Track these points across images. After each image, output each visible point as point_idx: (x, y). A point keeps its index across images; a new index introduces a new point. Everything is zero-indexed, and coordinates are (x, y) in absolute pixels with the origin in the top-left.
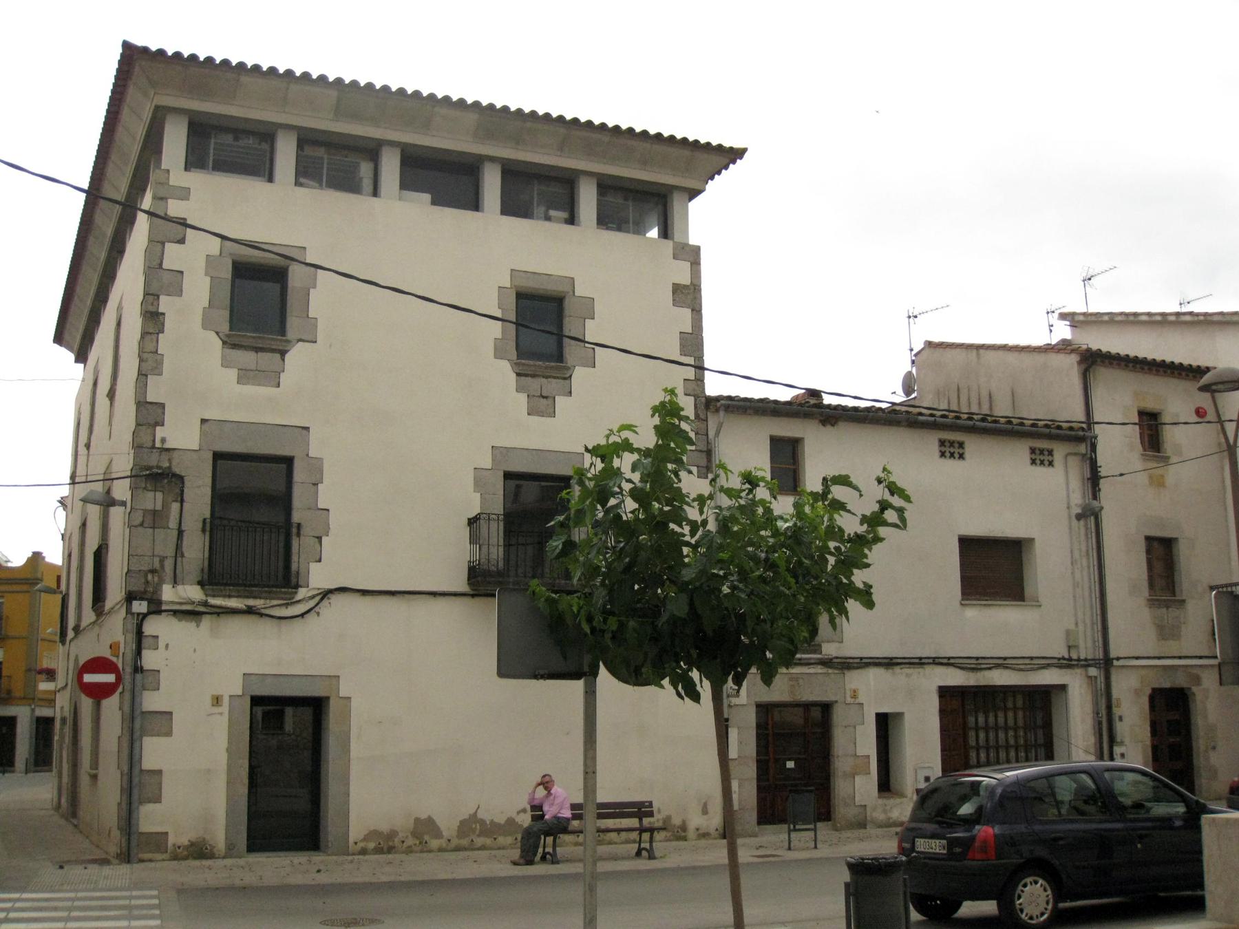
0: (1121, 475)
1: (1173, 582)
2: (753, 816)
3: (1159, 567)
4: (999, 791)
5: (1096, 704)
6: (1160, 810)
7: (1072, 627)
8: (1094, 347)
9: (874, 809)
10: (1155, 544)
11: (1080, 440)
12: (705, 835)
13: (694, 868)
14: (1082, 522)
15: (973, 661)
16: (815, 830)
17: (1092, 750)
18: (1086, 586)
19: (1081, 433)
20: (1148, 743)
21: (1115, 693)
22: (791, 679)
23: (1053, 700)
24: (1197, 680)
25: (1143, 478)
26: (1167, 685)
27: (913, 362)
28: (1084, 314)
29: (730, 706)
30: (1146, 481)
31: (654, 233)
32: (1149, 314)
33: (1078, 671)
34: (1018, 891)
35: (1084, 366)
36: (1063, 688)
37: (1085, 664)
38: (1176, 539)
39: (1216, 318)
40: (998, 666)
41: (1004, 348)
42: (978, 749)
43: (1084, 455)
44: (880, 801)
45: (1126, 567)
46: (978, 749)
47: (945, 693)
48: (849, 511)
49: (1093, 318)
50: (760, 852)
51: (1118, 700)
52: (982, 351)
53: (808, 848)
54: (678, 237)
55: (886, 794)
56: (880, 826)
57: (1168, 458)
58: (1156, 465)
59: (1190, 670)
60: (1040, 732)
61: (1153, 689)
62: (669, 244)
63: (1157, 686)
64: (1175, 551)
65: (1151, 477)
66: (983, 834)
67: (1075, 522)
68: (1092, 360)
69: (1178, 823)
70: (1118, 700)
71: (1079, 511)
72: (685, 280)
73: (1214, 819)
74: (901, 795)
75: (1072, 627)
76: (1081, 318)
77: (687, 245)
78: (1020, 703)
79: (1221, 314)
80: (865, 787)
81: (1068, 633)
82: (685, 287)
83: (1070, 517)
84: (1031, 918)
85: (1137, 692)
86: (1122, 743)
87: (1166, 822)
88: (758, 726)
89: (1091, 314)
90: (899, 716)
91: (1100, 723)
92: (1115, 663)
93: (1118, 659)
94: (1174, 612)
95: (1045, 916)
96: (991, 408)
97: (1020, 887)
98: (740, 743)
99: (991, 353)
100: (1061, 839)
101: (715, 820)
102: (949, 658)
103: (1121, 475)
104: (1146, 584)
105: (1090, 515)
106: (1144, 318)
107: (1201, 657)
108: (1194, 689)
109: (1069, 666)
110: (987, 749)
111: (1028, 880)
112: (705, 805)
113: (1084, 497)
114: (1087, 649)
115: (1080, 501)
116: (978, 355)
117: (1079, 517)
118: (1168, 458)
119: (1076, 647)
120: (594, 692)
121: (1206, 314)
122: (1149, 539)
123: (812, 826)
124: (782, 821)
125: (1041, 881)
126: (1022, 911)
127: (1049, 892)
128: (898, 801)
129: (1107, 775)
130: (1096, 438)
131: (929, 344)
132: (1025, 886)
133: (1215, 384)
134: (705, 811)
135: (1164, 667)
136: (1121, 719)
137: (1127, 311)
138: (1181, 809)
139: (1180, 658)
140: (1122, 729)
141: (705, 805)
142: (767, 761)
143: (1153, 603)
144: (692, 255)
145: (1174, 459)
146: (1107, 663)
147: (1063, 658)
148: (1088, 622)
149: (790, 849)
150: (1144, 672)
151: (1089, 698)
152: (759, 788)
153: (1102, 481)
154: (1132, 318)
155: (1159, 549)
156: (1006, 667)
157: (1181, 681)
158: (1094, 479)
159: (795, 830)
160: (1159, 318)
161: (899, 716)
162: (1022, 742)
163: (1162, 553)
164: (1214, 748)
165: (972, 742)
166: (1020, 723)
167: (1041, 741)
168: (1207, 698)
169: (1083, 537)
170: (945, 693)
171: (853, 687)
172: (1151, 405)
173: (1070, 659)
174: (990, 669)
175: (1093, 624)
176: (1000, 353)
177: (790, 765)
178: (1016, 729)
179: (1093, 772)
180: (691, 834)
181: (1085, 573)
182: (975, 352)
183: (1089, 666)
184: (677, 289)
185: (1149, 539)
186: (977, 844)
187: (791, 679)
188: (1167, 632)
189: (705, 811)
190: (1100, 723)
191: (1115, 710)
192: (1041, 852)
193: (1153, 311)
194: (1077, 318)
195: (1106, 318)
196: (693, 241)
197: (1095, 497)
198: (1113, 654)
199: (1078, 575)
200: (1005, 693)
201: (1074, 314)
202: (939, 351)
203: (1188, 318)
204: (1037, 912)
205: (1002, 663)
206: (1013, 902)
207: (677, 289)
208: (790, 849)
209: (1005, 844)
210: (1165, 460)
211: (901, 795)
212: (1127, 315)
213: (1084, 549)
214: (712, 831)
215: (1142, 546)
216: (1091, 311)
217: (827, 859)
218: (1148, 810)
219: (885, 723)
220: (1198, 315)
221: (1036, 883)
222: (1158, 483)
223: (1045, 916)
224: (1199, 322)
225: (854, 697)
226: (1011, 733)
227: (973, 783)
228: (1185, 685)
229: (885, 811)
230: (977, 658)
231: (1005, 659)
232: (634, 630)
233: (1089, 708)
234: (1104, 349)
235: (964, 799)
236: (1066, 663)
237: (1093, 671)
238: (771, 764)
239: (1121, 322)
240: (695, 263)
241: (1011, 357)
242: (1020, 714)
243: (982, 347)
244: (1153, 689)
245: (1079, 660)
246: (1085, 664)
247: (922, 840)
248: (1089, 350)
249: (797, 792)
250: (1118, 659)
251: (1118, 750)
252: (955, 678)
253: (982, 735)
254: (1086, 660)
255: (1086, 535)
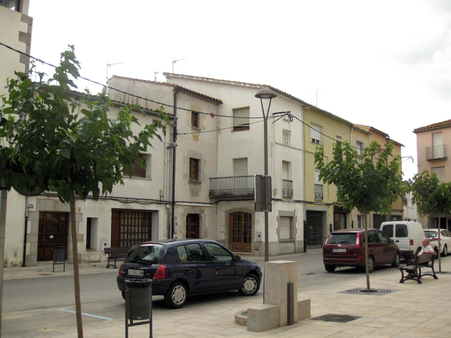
0: (185, 134)
1: (197, 176)
2: (35, 257)
3: (193, 169)
4: (166, 251)
5: (168, 218)
6: (220, 259)
7: (162, 189)
8: (180, 85)
9: (84, 255)
10: (192, 161)
11: (171, 119)
12: (15, 265)
13: (15, 280)
14: (169, 150)
15: (126, 199)
16: (64, 264)
17: (166, 235)
18: (168, 174)
19: (172, 117)
20: (185, 233)
21: (175, 215)
22: (54, 202)
23: (153, 215)
24: (203, 212)
25: (191, 136)
26: (193, 213)
27: (107, 82)
28: (173, 74)
29: (28, 212)
30: (192, 137)
31: (13, 9)
32: (197, 77)
33: (163, 206)
34: (173, 291)
35: (175, 92)
36: (157, 211)
37: (166, 203)
38: (200, 160)
39: (221, 82)
40: (134, 202)
41: (145, 81)
42: (124, 233)
43: (172, 125)
44: (87, 253)
45: (183, 168)
46: (124, 233)
47: (115, 211)
48: (138, 123)
49: (176, 76)
50: (41, 273)
51: (176, 217)
52: (136, 81)
53: (60, 271)
54: (24, 12)
55: (88, 250)
56: (86, 262)
57: (200, 130)
58: (195, 132)
59: (201, 208)
60: (147, 228)
61: (188, 214)
62: (19, 15)
63: (189, 213)
64: (199, 164)
65: (194, 137)
66: (159, 268)
67: (166, 149)
68: (178, 90)
69: (228, 264)
70: (176, 217)
71: (169, 146)
72: (25, 31)
73: (271, 263)
74: (95, 250)
75: (162, 189)
76: (172, 75)
77: (28, 16)
78: (140, 216)
79: (223, 80)
80: (81, 246)
81: (160, 191)
82: (24, 34)
83: (165, 148)
84: (177, 302)
85: (183, 215)
86: (176, 233)
87: (222, 264)
88: (40, 220)
89: (175, 74)
90: (96, 219)
91: (169, 225)
92: (176, 203)
93: (177, 202)
94: (197, 186)
95: (183, 301)
96: (137, 103)
97: (174, 290)
98: (32, 227)
99: (140, 83)
100: (190, 270)
101: (20, 259)
102: (117, 198)
103: (185, 134)
104: (188, 175)
105: (172, 148)
106: (195, 78)
107: (205, 203)
108: (202, 215)
109: (160, 204)
110: (127, 233)
111: (177, 287)
112: (16, 253)
113: (170, 141)
114: (167, 197)
115: (169, 142)
116: (134, 83)
117: (168, 148)
118: (200, 130)
119: (163, 196)
120: (6, 198)
121: (218, 80)
122: (191, 159)
123: (63, 262)
124: (51, 259)
125: (181, 287)
126: (174, 299)
127: (184, 292)
128: (94, 252)
129: (205, 244)
130: (177, 119)
131: (115, 76)
132: (176, 289)
133: (264, 94)
134: (15, 255)
135: (193, 206)
136: (176, 224)
137: (189, 75)
138: (230, 258)
139: (198, 203)
140: (177, 228)
141: (16, 253)
142: (42, 235)
143: (191, 182)
144: (29, 21)
145: (202, 131)
146: (173, 203)
147: (158, 200)
148: (168, 187)
149: (53, 271)
150: (185, 207)
151: (166, 216)
152: (39, 246)
153: (178, 135)
154: (190, 78)
155: (194, 163)
156: (137, 202)
157: (197, 212)
158: (175, 135)
159: (56, 264)
160: (200, 79)
161: (96, 219)
162: (140, 231)
163: (195, 163)
164: (206, 236)
165: (122, 231)
166: (140, 224)
167: (147, 231)
168: (205, 218)
169: (169, 156)
170: (115, 211)
171: (79, 207)
172: (196, 110)
173: (161, 201)
174: (131, 203)
175: (170, 188)
176: (143, 83)
177: (52, 237)
178: (138, 226)
179: (200, 243)
180: (9, 265)
181: (168, 169)
182: (133, 81)
183: (167, 204)
184: (21, 34)
185: (191, 159)
186: (157, 272)
187: (54, 202)
188: (194, 193)
189: (15, 255)
190: (169, 225)
191: (175, 221)
192: (181, 275)
193: (199, 76)
194: (170, 75)
195: (181, 77)
196: (30, 15)
197: (174, 141)
198: (176, 200)
199: (166, 168)
200: (124, 212)
201: (169, 73)
202: (119, 79)
203: (211, 80)
204: (179, 300)
205: (136, 201)
206: (171, 297)
207: (21, 34)
208: (53, 271)
209: (169, 272)
210: (199, 131)
211: (95, 250)
212: (189, 76)
213: (169, 159)
214: (18, 263)
215: (188, 161)
216: (175, 73)
217: (68, 276)
218: (216, 259)
219: (90, 221)
220: (215, 80)
221: (180, 288)
222: (196, 138)
223: (183, 301)
224: (215, 83)
225: (79, 211)
226: (136, 228)
227: (150, 247)
228: (199, 213)
229: (88, 256)
230: (127, 198)
231: (137, 199)
232: (39, 165)
233: (166, 220)
234: (183, 87)
235: (146, 253)
236: (159, 202)
237: (168, 206)
238: (44, 236)
239: (186, 79)
240: (30, 25)
241: (147, 85)
242: (140, 220)
243: (136, 80)
244: (188, 214)
245: (164, 201)
246: (166, 203)
247: (132, 270)
248: (178, 86)
249: (58, 248)
250: (177, 202)
251: (175, 236)
252: (118, 205)
253: (126, 228)
254: (166, 202)
255: (170, 155)
